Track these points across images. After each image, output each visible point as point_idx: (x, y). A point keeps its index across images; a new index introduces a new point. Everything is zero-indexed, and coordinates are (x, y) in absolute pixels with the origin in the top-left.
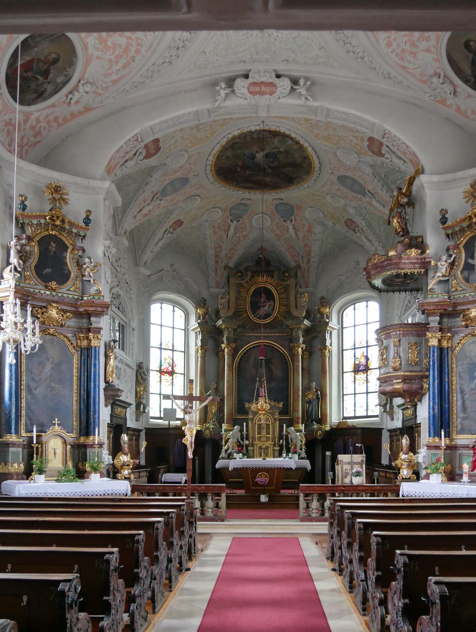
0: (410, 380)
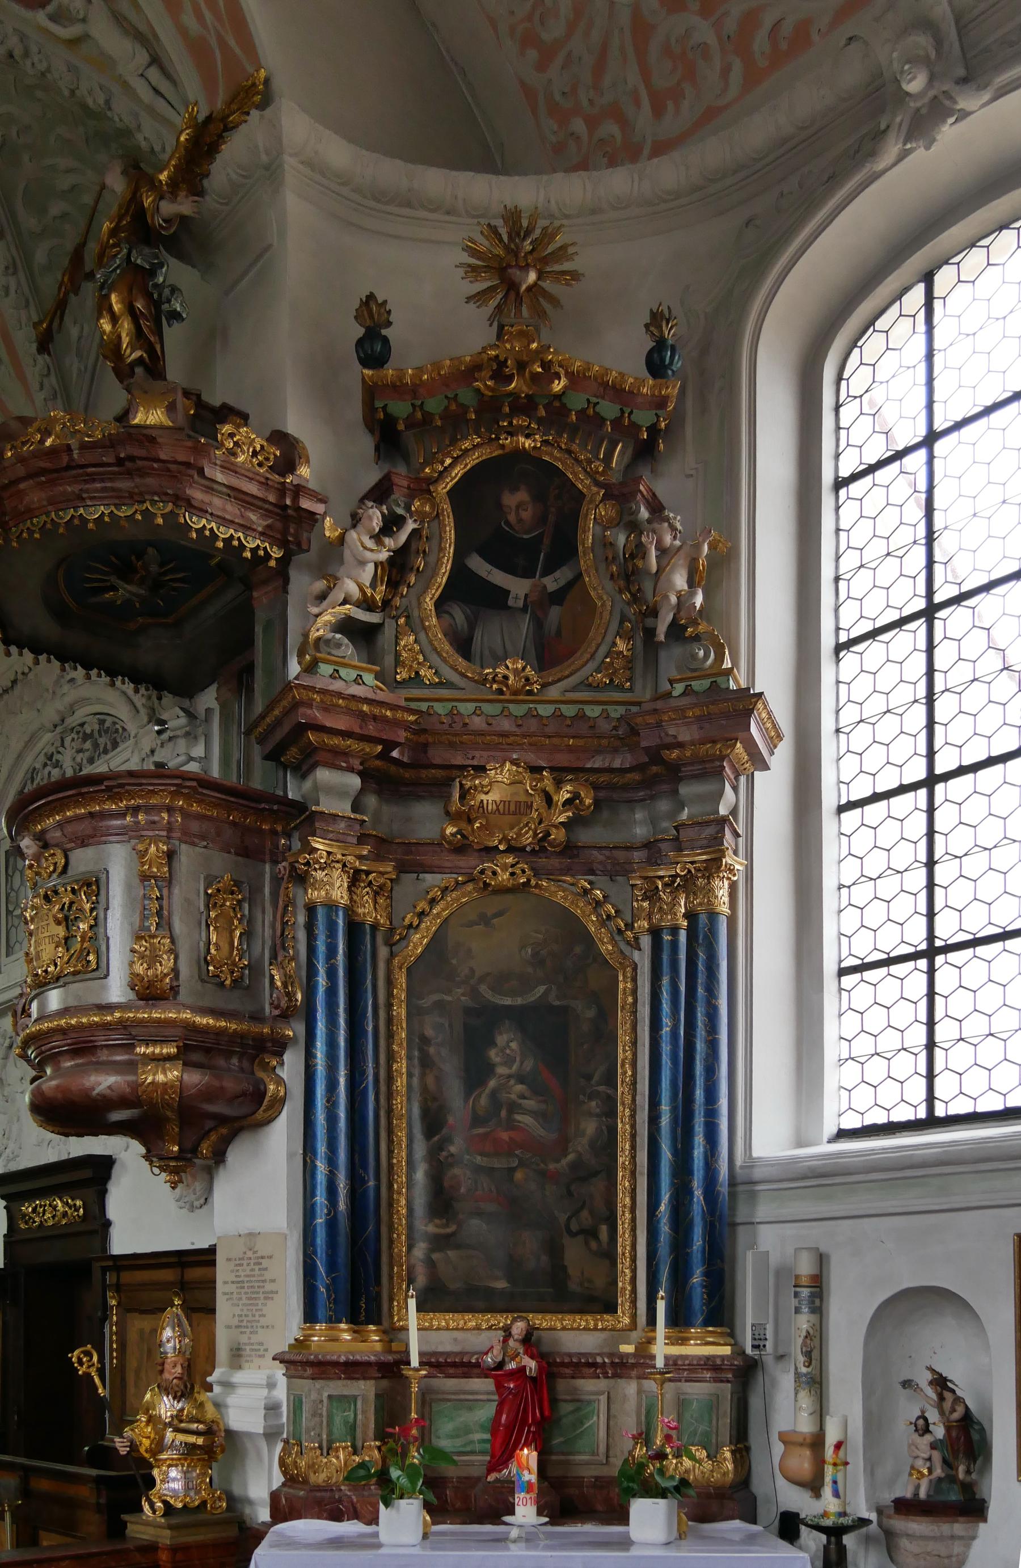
0: (208, 1051)
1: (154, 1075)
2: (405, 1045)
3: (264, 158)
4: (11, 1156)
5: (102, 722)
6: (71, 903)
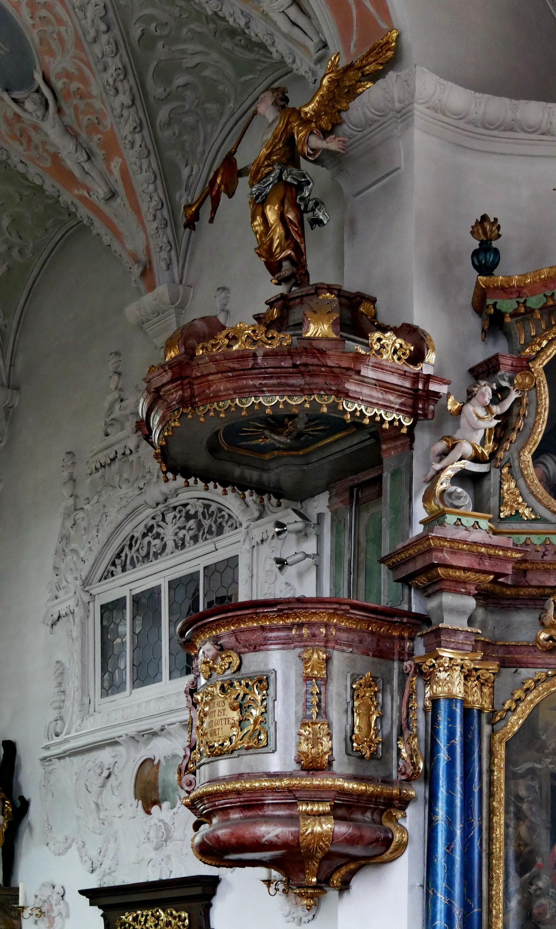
1: (313, 827)
2: (503, 802)
3: (398, 105)
4: (108, 871)
5: (207, 507)
6: (245, 695)
